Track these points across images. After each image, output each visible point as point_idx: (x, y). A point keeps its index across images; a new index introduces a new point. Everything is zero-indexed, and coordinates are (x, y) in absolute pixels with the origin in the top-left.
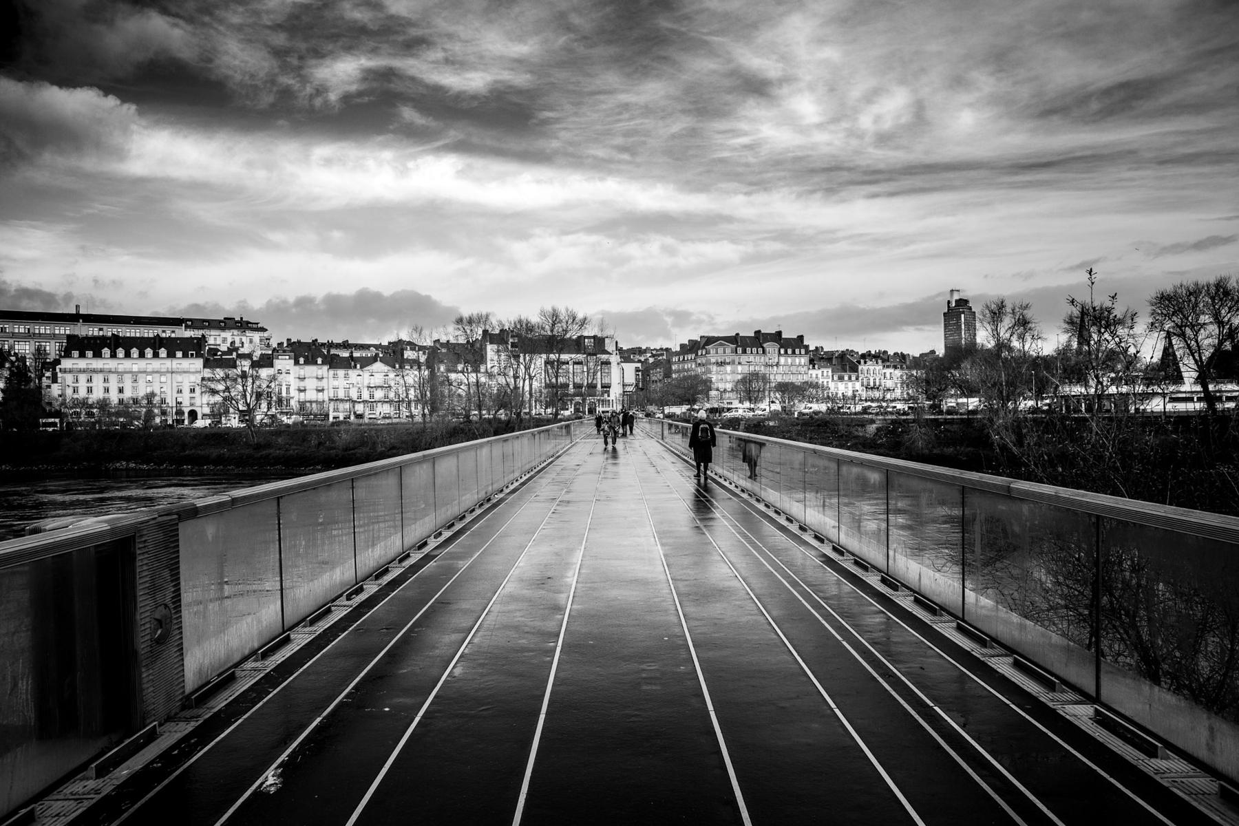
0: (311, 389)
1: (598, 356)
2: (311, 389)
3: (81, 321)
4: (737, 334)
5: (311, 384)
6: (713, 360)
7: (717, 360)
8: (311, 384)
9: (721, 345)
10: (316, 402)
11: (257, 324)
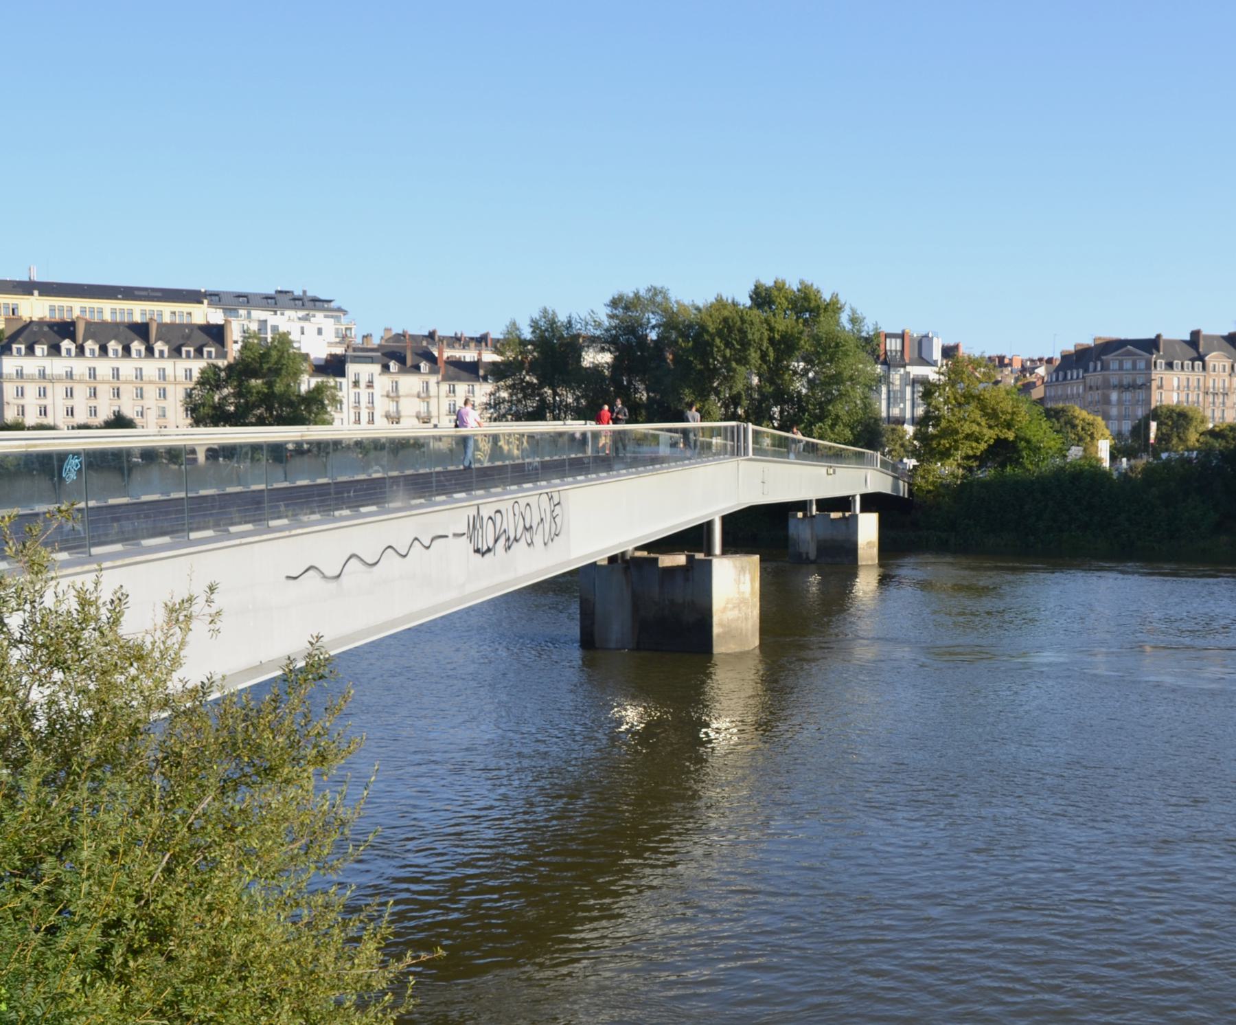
0: (407, 396)
1: (909, 368)
2: (407, 396)
3: (36, 292)
4: (1158, 336)
5: (410, 407)
6: (1114, 380)
7: (1121, 381)
8: (410, 407)
9: (1129, 354)
10: (49, 512)
11: (330, 301)
